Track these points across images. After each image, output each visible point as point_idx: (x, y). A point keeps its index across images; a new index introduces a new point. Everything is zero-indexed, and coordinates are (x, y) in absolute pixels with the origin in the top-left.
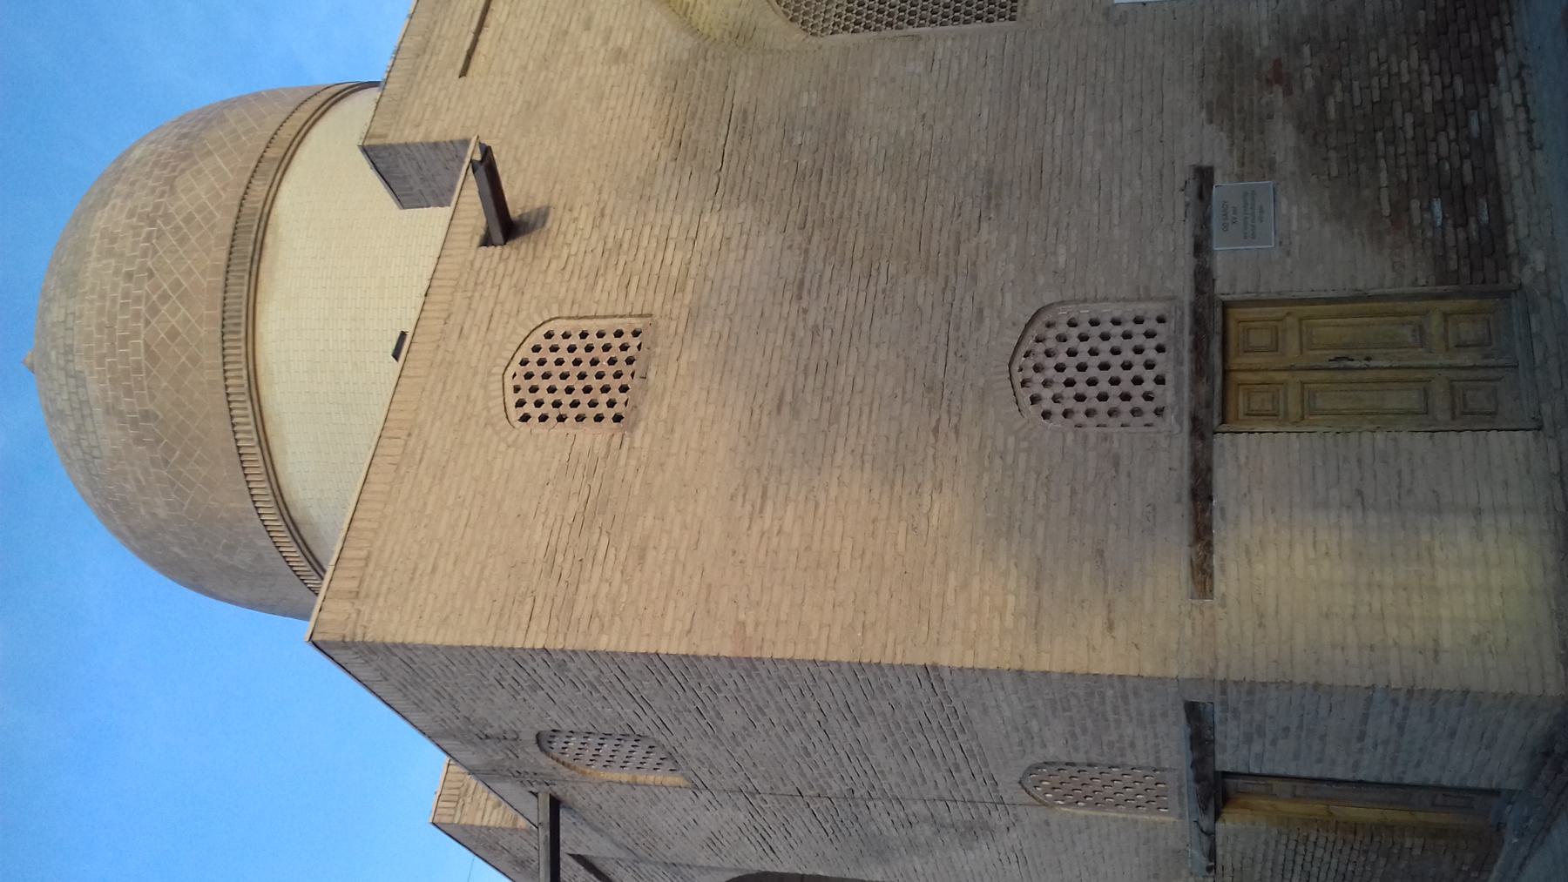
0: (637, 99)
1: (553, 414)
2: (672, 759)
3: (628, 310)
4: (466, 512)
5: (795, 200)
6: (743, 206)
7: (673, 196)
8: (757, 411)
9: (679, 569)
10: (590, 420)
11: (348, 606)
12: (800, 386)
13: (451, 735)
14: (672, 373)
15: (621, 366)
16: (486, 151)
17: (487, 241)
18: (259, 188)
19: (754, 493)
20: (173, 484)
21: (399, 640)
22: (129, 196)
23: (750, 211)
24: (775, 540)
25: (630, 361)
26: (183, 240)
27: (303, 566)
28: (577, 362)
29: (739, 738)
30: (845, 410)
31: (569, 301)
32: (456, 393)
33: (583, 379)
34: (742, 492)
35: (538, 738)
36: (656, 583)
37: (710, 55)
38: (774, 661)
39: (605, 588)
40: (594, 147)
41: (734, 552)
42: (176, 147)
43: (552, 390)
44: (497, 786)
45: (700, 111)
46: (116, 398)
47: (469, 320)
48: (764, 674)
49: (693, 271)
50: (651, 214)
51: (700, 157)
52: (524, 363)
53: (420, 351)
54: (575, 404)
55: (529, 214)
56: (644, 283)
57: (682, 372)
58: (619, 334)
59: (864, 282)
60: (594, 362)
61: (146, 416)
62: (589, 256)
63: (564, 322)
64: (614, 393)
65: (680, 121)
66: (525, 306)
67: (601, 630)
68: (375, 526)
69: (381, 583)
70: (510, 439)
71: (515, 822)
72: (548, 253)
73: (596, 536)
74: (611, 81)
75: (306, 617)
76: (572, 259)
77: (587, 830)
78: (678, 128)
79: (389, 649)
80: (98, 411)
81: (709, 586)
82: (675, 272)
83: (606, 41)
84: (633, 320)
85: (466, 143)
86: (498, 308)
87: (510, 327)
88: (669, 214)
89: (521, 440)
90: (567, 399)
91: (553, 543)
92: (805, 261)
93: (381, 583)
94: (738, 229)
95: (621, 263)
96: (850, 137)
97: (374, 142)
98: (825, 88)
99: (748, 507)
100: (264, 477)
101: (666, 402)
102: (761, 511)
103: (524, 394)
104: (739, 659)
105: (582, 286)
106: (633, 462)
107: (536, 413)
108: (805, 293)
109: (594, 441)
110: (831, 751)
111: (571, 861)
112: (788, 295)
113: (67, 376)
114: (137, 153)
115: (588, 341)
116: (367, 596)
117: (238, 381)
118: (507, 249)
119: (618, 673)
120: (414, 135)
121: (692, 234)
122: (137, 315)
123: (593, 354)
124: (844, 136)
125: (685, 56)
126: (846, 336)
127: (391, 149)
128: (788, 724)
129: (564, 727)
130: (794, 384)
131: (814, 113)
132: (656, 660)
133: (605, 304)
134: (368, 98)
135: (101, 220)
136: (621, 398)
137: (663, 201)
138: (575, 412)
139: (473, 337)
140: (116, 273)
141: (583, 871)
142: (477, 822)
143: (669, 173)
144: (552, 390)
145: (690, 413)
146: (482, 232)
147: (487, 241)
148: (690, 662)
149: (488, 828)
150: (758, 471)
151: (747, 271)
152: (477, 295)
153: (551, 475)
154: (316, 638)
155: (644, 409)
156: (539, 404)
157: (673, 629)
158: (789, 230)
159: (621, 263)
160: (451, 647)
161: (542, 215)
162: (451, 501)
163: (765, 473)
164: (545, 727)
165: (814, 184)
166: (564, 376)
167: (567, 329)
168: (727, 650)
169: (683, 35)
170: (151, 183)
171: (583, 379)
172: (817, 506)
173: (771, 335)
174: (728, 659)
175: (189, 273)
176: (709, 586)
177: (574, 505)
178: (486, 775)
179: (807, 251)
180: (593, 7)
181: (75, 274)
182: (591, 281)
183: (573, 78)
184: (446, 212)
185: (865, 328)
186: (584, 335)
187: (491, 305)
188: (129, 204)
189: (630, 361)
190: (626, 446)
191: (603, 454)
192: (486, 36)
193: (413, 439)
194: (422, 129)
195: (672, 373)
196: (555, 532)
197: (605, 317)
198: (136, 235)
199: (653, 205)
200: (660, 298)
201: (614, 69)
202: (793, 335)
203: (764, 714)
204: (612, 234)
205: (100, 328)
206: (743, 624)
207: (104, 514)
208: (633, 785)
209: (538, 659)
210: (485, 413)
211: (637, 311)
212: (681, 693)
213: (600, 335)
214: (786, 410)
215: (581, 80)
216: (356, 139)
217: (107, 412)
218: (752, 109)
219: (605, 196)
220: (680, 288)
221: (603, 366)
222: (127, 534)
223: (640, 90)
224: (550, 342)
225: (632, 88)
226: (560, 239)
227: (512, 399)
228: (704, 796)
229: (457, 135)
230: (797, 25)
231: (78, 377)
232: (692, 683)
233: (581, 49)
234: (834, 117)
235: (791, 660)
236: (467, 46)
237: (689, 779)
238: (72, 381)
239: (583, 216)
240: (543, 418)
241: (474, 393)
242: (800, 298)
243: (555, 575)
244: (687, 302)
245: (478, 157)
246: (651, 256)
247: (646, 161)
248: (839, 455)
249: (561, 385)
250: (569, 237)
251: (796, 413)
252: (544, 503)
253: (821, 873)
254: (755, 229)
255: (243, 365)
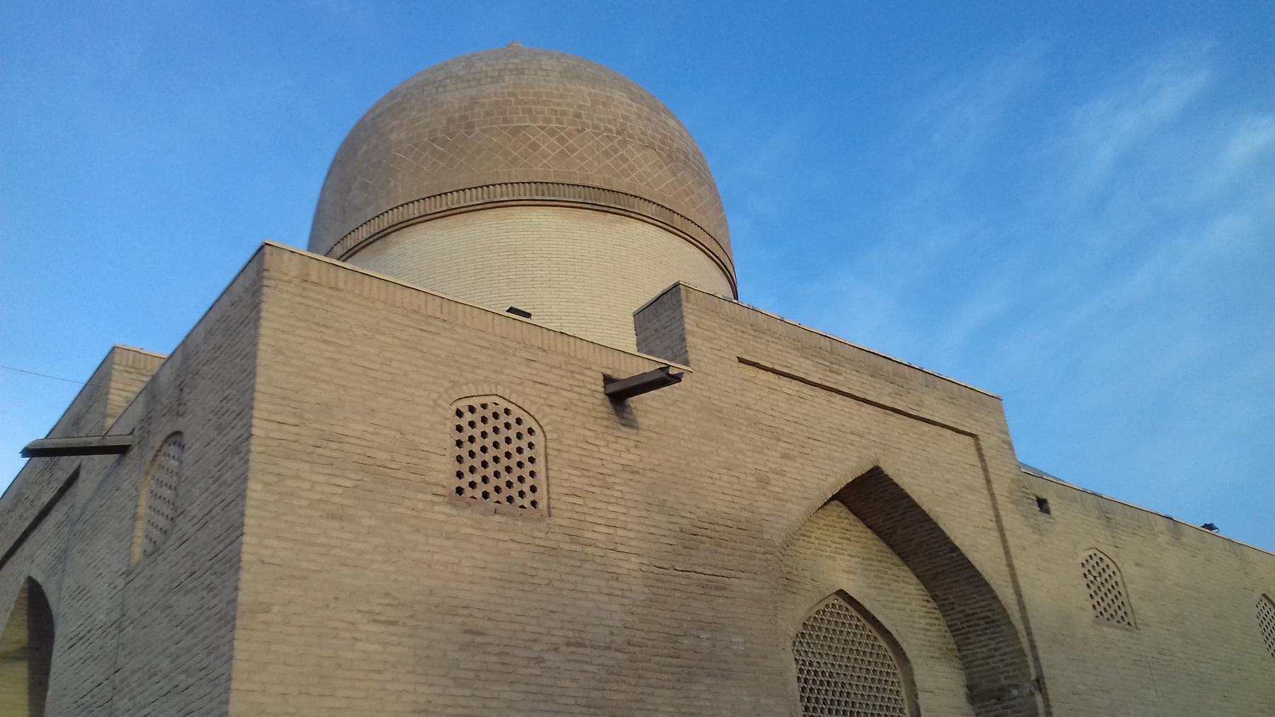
0: (729, 498)
1: (464, 437)
2: (154, 551)
3: (553, 496)
4: (377, 367)
5: (653, 636)
6: (646, 590)
7: (652, 530)
8: (467, 612)
9: (322, 550)
10: (458, 467)
11: (295, 273)
12: (490, 649)
13: (186, 359)
14: (500, 536)
15: (506, 492)
16: (677, 378)
17: (608, 380)
18: (650, 210)
19: (391, 614)
20: (416, 145)
21: (263, 314)
22: (640, 117)
23: (642, 597)
24: (347, 635)
25: (510, 499)
26: (607, 154)
27: (350, 243)
28: (508, 455)
29: (167, 612)
30: (468, 692)
31: (560, 447)
32: (479, 357)
33: (493, 460)
34: (393, 602)
35: (177, 433)
36: (310, 530)
37: (769, 556)
38: (231, 641)
39: (306, 485)
40: (688, 465)
41: (336, 599)
42: (678, 150)
43: (484, 435)
44: (141, 399)
45: (723, 550)
46: (483, 105)
47: (541, 366)
48: (221, 633)
49: (589, 550)
50: (635, 513)
51: (685, 551)
52: (507, 412)
53: (517, 328)
54: (472, 454)
55: (631, 413)
56: (578, 509)
57: (501, 545)
58: (533, 489)
59: (584, 702)
60: (508, 469)
61: (470, 126)
62: (599, 462)
63: (543, 444)
64: (482, 488)
65: (714, 534)
66: (555, 411)
67: (266, 484)
68: (366, 295)
69: (315, 300)
70: (440, 402)
71: (111, 416)
72: (599, 429)
73: (353, 476)
74: (743, 476)
75: (310, 249)
76: (595, 448)
77: (99, 479)
78: (708, 533)
79: (256, 307)
80: (472, 92)
81: (305, 578)
82: (587, 534)
83: (774, 472)
84: (545, 501)
85: (686, 363)
86: (553, 390)
87: (538, 400)
88: (637, 528)
89: (440, 410)
90: (476, 448)
91: (348, 440)
92: (599, 648)
93: (315, 300)
94: (626, 587)
95: (594, 489)
96: (708, 681)
97: (683, 293)
98: (748, 656)
99: (378, 609)
100: (423, 213)
101: (475, 532)
102: (375, 621)
103: (480, 412)
104: (235, 609)
105: (573, 457)
106: (420, 505)
107: (464, 422)
108: (572, 649)
109: (440, 471)
110: (151, 699)
111: (75, 466)
112: (570, 634)
113: (500, 71)
114: (672, 123)
115: (527, 463)
116: (304, 288)
117: (498, 194)
118: (602, 396)
119: (228, 500)
120: (690, 322)
121: (621, 548)
122: (549, 121)
123: (503, 473)
124: (709, 675)
125: (766, 536)
126: (534, 689)
127: (678, 306)
128: (178, 657)
129: (186, 455)
130: (490, 644)
131: (727, 647)
132: (237, 533)
133: (558, 478)
134: (724, 289)
135: (620, 96)
136: (478, 493)
137: (647, 522)
138: (465, 454)
139: (529, 370)
140: (580, 107)
141: (66, 476)
142: (113, 384)
143: (671, 526)
144: (484, 435)
145: (465, 551)
146: (615, 376)
147: (608, 380)
148: (235, 564)
149: (107, 393)
150: (412, 616)
151: (591, 596)
152: (563, 373)
153: (409, 437)
154: (267, 249)
155: (467, 513)
156: (472, 424)
157: (266, 547)
158: (626, 632)
159: (594, 489)
160: (255, 357)
161: (630, 423)
162: (388, 355)
163: (411, 622)
164: (187, 438)
165: (666, 652)
166: (496, 445)
167: (536, 447)
168: (244, 597)
169: (783, 534)
170: (650, 132)
171: (493, 460)
172: (380, 672)
173: (534, 621)
174: (235, 600)
175: (583, 159)
176: (305, 578)
177: (382, 456)
178: (151, 391)
179: (609, 648)
180: (799, 460)
181: (578, 77)
182: (577, 465)
183: (744, 446)
184: (633, 349)
185: (543, 706)
186: (532, 460)
187: (555, 384)
188: (632, 117)
189: (510, 499)
190: (436, 499)
191: (427, 479)
192: (771, 377)
193: (440, 324)
194: (696, 329)
195: (500, 536)
196: (359, 442)
197: (547, 477)
198: (609, 121)
199: (643, 513)
200: (564, 522)
201: (751, 478)
202: (535, 641)
203: (187, 634)
204: (617, 480)
205: (538, 94)
206: (267, 610)
207: (393, 95)
208: (134, 517)
209: (243, 431)
210: (463, 380)
211: (553, 504)
212: (210, 556)
213: (532, 474)
214: (468, 638)
215: (741, 452)
216: (683, 279)
217: (472, 98)
218: (725, 593)
219: (649, 474)
220: (574, 539)
221: (506, 477)
222: (377, 112)
223: (736, 500)
224: (525, 433)
225: (738, 493)
226: (611, 438)
227: (476, 402)
228: (121, 582)
229: (692, 356)
230: (800, 628)
231: (498, 78)
232: (216, 566)
233: (766, 451)
234: (723, 666)
235: (231, 658)
236: (762, 363)
237: (137, 565)
238: (496, 73)
239: (632, 457)
240: (459, 429)
241: (481, 372)
242: (569, 644)
243: (318, 442)
244: (562, 545)
245: (672, 372)
246: (600, 514)
247: (680, 507)
248: (425, 689)
249: (488, 442)
250: (615, 446)
251: (464, 647)
252: (385, 432)
253: (49, 693)
254: (626, 602)
255: (512, 198)
